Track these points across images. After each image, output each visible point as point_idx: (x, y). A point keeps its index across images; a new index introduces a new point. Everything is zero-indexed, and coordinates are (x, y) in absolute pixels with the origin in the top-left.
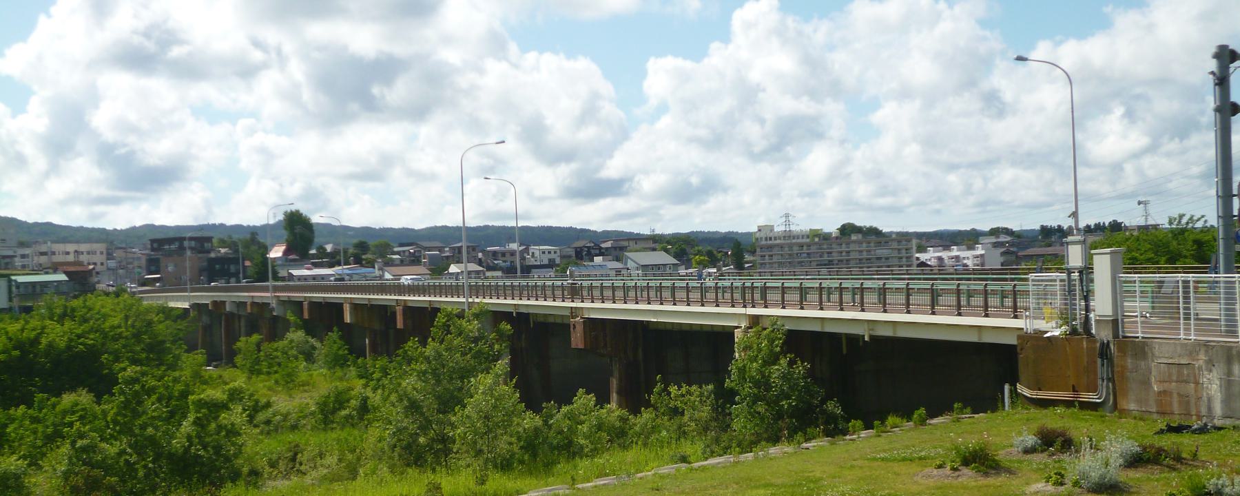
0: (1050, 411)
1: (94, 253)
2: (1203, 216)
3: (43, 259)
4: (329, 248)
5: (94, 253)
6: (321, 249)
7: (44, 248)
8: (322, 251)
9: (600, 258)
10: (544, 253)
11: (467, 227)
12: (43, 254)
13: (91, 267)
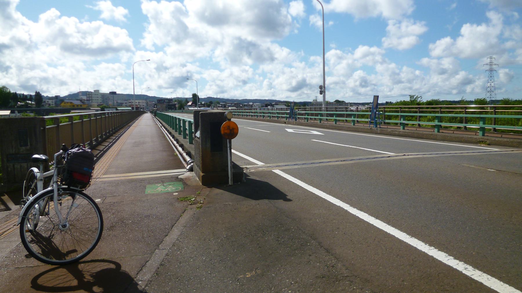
0: (336, 161)
1: (143, 103)
2: (421, 97)
3: (130, 104)
4: (203, 103)
5: (143, 103)
6: (201, 103)
7: (130, 101)
8: (201, 104)
9: (270, 107)
10: (257, 105)
11: (136, 95)
12: (130, 103)
13: (139, 106)
